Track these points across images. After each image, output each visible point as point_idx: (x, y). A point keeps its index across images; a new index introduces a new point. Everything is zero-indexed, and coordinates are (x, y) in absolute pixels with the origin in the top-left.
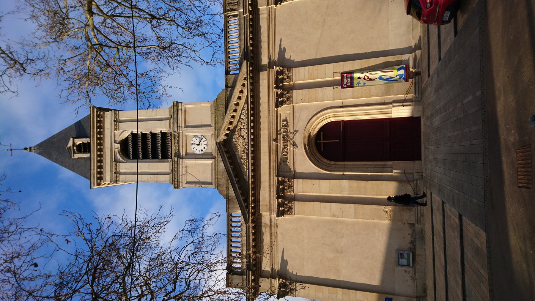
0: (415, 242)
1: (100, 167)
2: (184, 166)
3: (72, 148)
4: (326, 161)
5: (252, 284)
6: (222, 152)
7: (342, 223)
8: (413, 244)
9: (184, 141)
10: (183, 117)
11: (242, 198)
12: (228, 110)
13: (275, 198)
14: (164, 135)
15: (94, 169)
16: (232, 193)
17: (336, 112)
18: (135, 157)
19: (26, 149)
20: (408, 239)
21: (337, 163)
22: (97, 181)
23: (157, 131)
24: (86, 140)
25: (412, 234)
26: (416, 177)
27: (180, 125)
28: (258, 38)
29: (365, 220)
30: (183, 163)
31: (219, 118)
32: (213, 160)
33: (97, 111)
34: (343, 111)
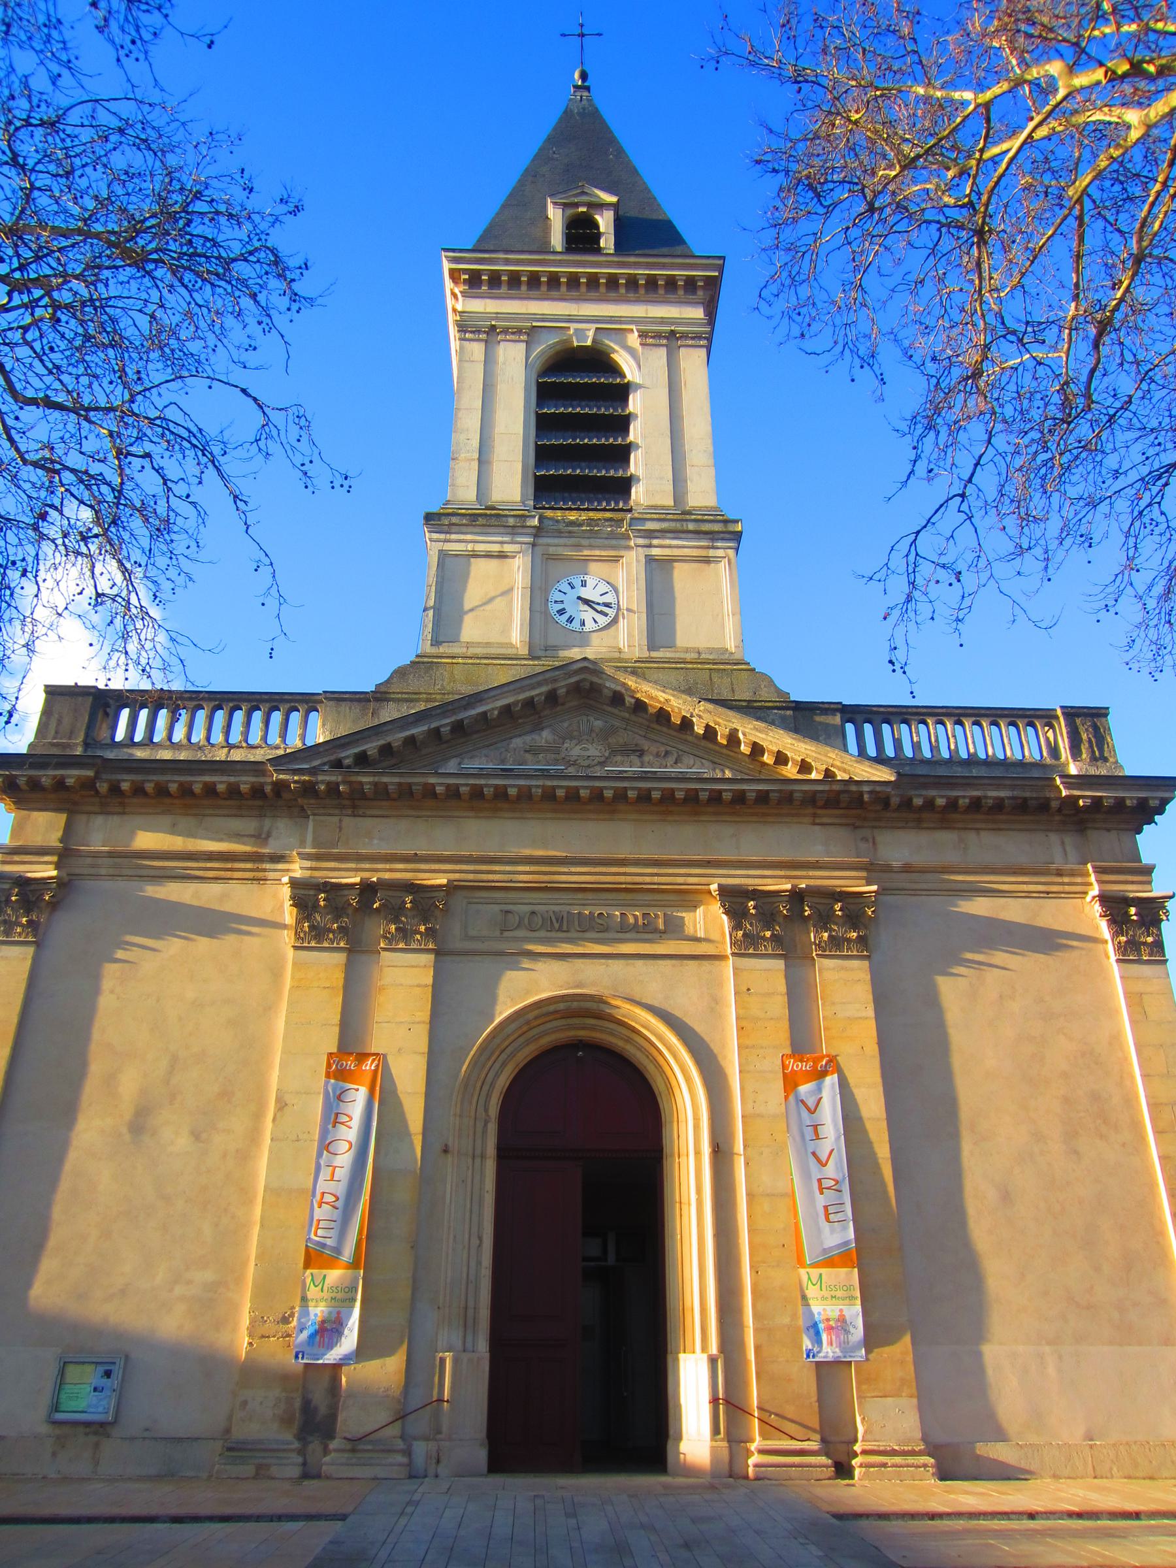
1: (514, 280)
2: (508, 548)
3: (584, 199)
4: (504, 1081)
5: (47, 777)
6: (555, 680)
7: (254, 1136)
11: (371, 747)
12: (710, 706)
13: (366, 875)
14: (624, 486)
15: (507, 262)
16: (389, 712)
17: (697, 1127)
18: (545, 392)
19: (584, 76)
21: (492, 1128)
22: (465, 271)
23: (636, 464)
24: (607, 242)
26: (420, 1449)
27: (655, 542)
29: (256, 1229)
30: (516, 547)
32: (524, 651)
33: (708, 279)
34: (698, 1153)
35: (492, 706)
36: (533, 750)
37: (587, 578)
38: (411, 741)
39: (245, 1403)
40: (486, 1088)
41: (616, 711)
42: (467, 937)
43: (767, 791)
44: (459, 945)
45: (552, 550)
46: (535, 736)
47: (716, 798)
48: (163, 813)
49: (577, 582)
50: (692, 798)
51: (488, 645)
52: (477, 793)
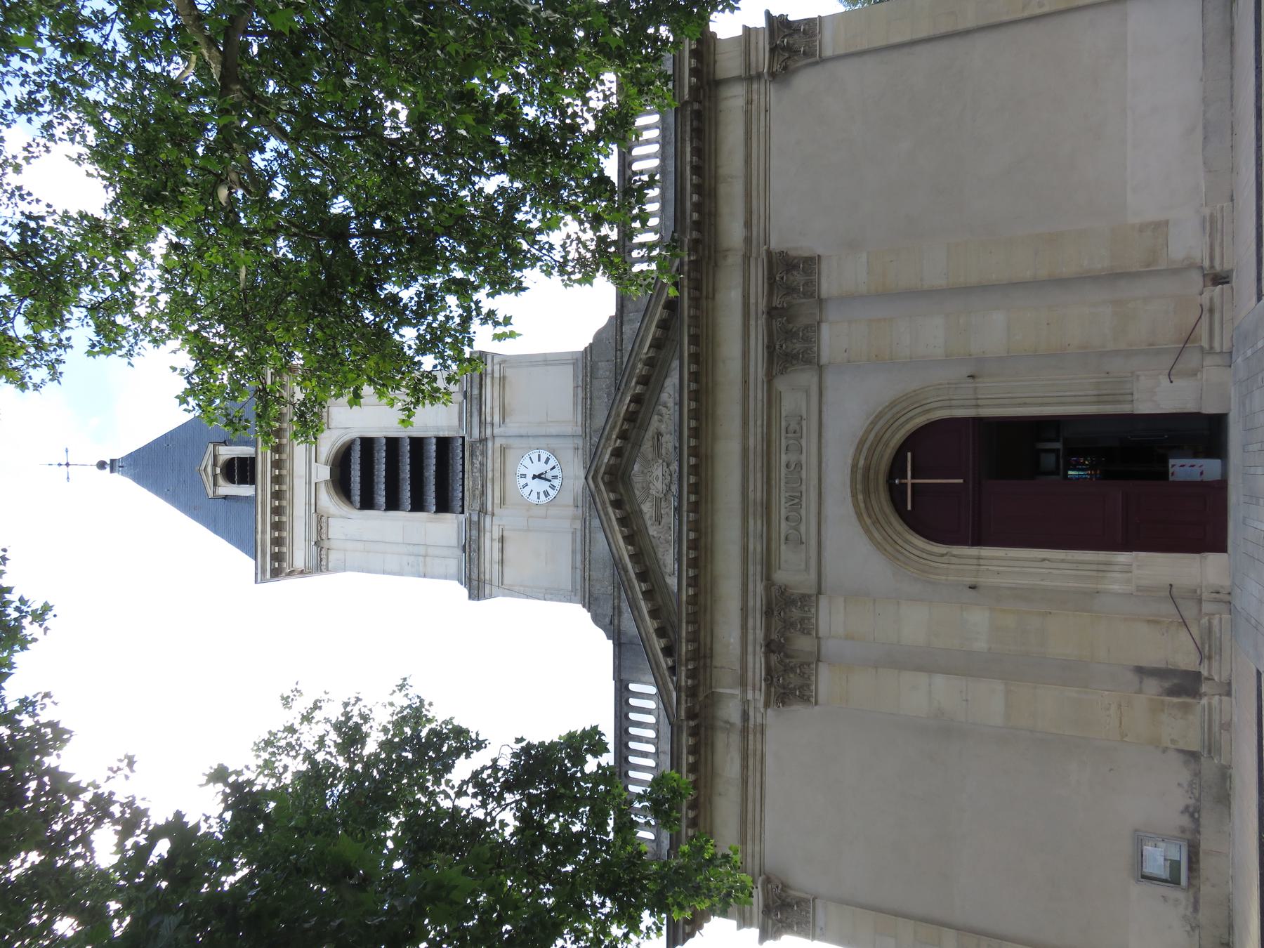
0: (1197, 809)
2: (496, 535)
6: (603, 502)
8: (1192, 815)
9: (497, 465)
10: (496, 394)
14: (444, 444)
15: (263, 532)
20: (1180, 799)
21: (957, 550)
25: (1191, 784)
27: (489, 419)
28: (716, 167)
30: (495, 529)
31: (596, 401)
35: (625, 551)
36: (659, 519)
37: (519, 473)
38: (654, 614)
39: (1173, 741)
40: (924, 556)
41: (627, 454)
42: (807, 569)
43: (689, 336)
44: (813, 576)
45: (497, 501)
46: (647, 517)
47: (695, 377)
48: (711, 803)
49: (523, 481)
50: (696, 396)
51: (574, 552)
52: (694, 563)
